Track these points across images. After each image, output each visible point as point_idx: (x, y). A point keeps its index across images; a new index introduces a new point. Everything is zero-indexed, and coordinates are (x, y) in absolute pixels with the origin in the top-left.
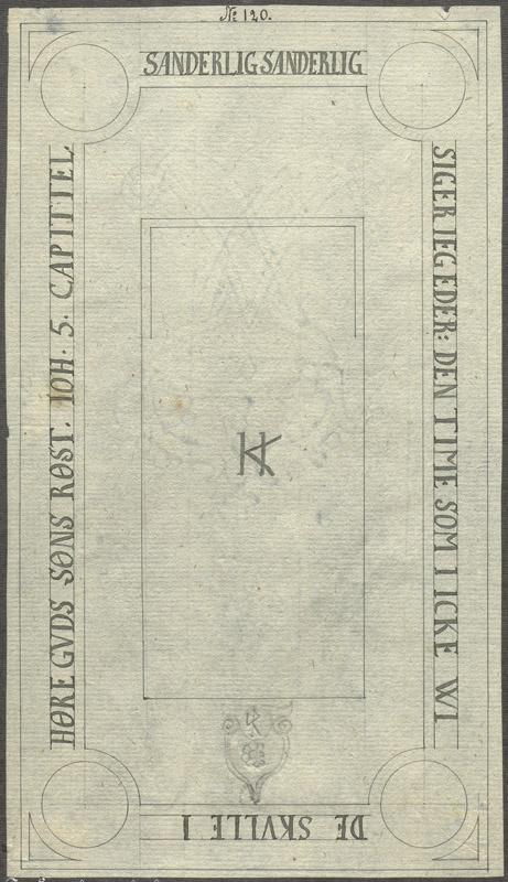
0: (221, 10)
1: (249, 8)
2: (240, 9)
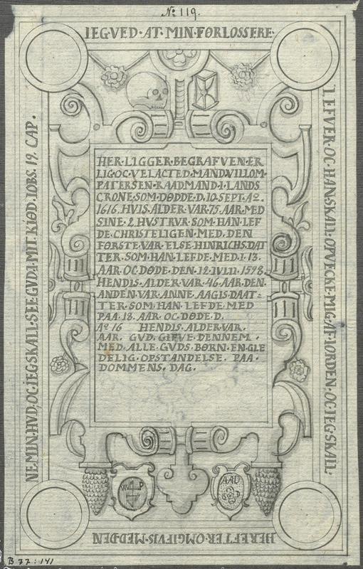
0: (163, 9)
1: (185, 7)
2: (177, 8)
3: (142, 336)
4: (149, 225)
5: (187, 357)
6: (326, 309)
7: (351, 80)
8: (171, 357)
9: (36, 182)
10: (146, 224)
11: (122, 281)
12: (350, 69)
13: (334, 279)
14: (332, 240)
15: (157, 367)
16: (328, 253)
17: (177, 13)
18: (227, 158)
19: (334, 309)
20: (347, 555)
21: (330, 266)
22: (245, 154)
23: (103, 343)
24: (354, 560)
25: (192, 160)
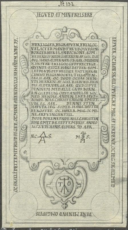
0: (59, 3)
1: (68, 2)
2: (65, 2)
3: (38, 99)
4: (39, 65)
5: (81, 85)
6: (112, 112)
7: (117, 170)
8: (70, 93)
9: (17, 50)
10: (38, 64)
11: (63, 48)
12: (125, 77)
13: (115, 101)
14: (114, 86)
15: (75, 100)
16: (114, 45)
17: (65, 4)
18: (116, 47)
19: (115, 113)
20: (122, 223)
21: (114, 95)
22: (89, 43)
23: (33, 95)
24: (126, 4)
25: (62, 44)
